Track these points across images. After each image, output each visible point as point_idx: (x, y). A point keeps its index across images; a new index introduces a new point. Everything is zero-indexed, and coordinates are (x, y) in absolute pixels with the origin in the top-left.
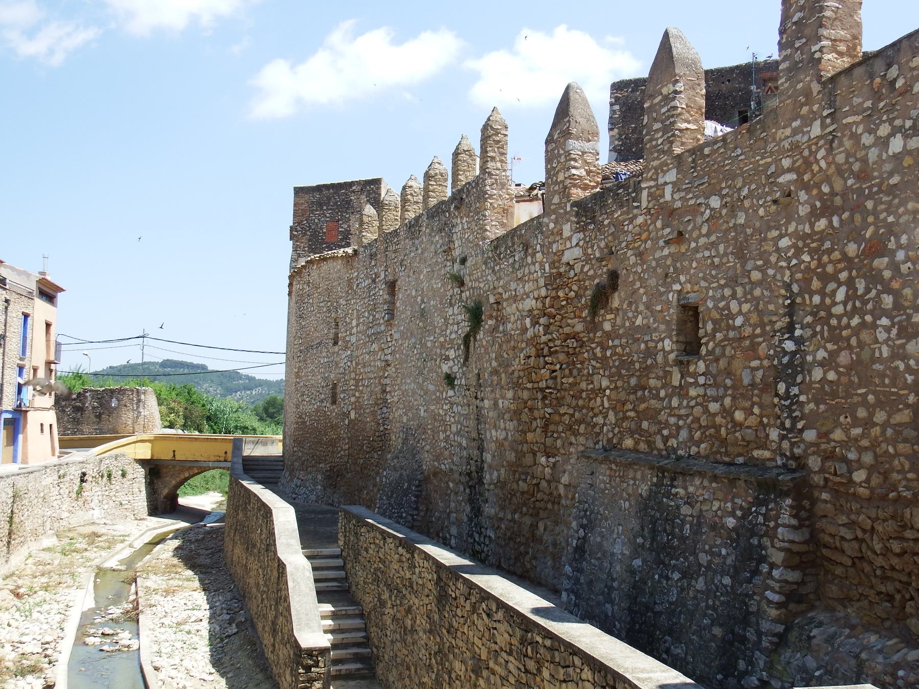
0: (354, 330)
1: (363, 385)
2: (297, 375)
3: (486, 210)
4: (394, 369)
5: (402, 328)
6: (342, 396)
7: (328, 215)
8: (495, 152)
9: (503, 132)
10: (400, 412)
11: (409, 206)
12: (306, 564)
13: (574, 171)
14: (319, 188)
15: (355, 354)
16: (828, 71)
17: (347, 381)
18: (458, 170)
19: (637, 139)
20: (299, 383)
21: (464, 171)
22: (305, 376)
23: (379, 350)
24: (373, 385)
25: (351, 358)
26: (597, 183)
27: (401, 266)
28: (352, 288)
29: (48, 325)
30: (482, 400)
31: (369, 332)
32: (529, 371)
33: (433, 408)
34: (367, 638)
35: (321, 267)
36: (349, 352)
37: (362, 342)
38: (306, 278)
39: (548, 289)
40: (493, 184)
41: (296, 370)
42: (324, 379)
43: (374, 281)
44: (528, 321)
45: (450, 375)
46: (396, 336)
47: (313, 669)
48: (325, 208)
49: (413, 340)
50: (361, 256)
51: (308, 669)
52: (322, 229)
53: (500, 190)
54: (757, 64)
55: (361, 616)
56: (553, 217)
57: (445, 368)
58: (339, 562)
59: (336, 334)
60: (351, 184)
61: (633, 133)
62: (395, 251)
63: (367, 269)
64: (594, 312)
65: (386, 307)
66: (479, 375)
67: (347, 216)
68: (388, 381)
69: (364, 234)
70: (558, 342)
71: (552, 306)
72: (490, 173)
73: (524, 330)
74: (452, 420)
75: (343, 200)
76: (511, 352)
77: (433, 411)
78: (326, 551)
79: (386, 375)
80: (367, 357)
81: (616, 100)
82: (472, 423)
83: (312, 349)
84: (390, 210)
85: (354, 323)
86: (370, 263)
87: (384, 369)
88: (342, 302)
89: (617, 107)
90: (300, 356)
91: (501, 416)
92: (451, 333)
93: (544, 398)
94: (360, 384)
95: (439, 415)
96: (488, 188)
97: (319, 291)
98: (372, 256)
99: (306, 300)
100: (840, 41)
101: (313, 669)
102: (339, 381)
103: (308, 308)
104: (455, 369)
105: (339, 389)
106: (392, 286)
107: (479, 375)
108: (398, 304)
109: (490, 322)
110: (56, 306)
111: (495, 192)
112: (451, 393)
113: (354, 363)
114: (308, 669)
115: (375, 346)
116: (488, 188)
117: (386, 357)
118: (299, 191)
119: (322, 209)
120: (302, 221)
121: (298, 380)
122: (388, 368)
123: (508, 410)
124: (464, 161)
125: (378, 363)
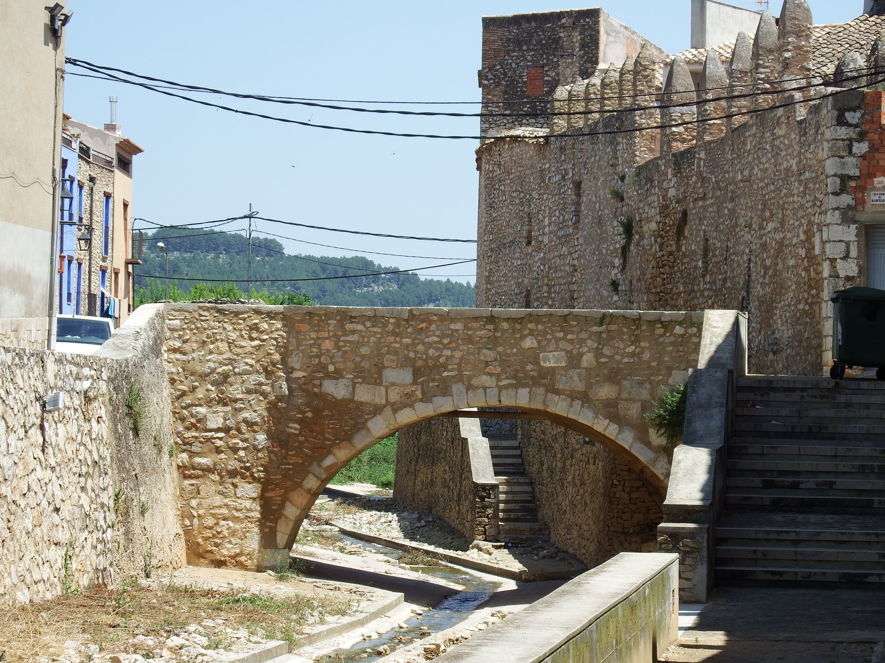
0: (547, 230)
1: (555, 292)
2: (488, 281)
3: (636, 137)
4: (579, 275)
5: (585, 233)
7: (529, 58)
8: (644, 86)
9: (650, 67)
11: (592, 105)
12: (485, 442)
14: (517, 20)
15: (547, 257)
16: (735, 125)
18: (623, 90)
20: (490, 290)
22: (497, 281)
23: (568, 254)
24: (563, 292)
26: (694, 137)
28: (544, 181)
29: (126, 206)
30: (633, 303)
31: (561, 233)
32: (654, 278)
34: (534, 497)
35: (512, 147)
37: (553, 243)
38: (497, 158)
39: (661, 216)
40: (642, 114)
41: (487, 274)
42: (519, 285)
44: (653, 239)
45: (615, 281)
47: (486, 499)
48: (525, 48)
50: (552, 146)
51: (482, 499)
52: (521, 77)
53: (649, 119)
55: (531, 484)
56: (664, 161)
58: (518, 452)
59: (530, 232)
60: (560, 15)
62: (581, 151)
63: (557, 162)
64: (679, 240)
65: (573, 209)
67: (555, 60)
68: (575, 287)
69: (556, 121)
70: (665, 258)
75: (549, 38)
78: (505, 443)
83: (505, 248)
85: (547, 221)
86: (561, 157)
88: (535, 195)
90: (491, 256)
93: (660, 300)
96: (637, 118)
97: (511, 177)
99: (497, 186)
100: (743, 107)
101: (486, 499)
102: (532, 287)
103: (499, 197)
105: (533, 297)
106: (578, 185)
108: (583, 208)
110: (131, 177)
111: (644, 121)
112: (616, 298)
113: (547, 266)
114: (482, 499)
116: (637, 118)
118: (489, 24)
119: (521, 50)
120: (495, 66)
121: (489, 286)
122: (576, 274)
125: (567, 268)
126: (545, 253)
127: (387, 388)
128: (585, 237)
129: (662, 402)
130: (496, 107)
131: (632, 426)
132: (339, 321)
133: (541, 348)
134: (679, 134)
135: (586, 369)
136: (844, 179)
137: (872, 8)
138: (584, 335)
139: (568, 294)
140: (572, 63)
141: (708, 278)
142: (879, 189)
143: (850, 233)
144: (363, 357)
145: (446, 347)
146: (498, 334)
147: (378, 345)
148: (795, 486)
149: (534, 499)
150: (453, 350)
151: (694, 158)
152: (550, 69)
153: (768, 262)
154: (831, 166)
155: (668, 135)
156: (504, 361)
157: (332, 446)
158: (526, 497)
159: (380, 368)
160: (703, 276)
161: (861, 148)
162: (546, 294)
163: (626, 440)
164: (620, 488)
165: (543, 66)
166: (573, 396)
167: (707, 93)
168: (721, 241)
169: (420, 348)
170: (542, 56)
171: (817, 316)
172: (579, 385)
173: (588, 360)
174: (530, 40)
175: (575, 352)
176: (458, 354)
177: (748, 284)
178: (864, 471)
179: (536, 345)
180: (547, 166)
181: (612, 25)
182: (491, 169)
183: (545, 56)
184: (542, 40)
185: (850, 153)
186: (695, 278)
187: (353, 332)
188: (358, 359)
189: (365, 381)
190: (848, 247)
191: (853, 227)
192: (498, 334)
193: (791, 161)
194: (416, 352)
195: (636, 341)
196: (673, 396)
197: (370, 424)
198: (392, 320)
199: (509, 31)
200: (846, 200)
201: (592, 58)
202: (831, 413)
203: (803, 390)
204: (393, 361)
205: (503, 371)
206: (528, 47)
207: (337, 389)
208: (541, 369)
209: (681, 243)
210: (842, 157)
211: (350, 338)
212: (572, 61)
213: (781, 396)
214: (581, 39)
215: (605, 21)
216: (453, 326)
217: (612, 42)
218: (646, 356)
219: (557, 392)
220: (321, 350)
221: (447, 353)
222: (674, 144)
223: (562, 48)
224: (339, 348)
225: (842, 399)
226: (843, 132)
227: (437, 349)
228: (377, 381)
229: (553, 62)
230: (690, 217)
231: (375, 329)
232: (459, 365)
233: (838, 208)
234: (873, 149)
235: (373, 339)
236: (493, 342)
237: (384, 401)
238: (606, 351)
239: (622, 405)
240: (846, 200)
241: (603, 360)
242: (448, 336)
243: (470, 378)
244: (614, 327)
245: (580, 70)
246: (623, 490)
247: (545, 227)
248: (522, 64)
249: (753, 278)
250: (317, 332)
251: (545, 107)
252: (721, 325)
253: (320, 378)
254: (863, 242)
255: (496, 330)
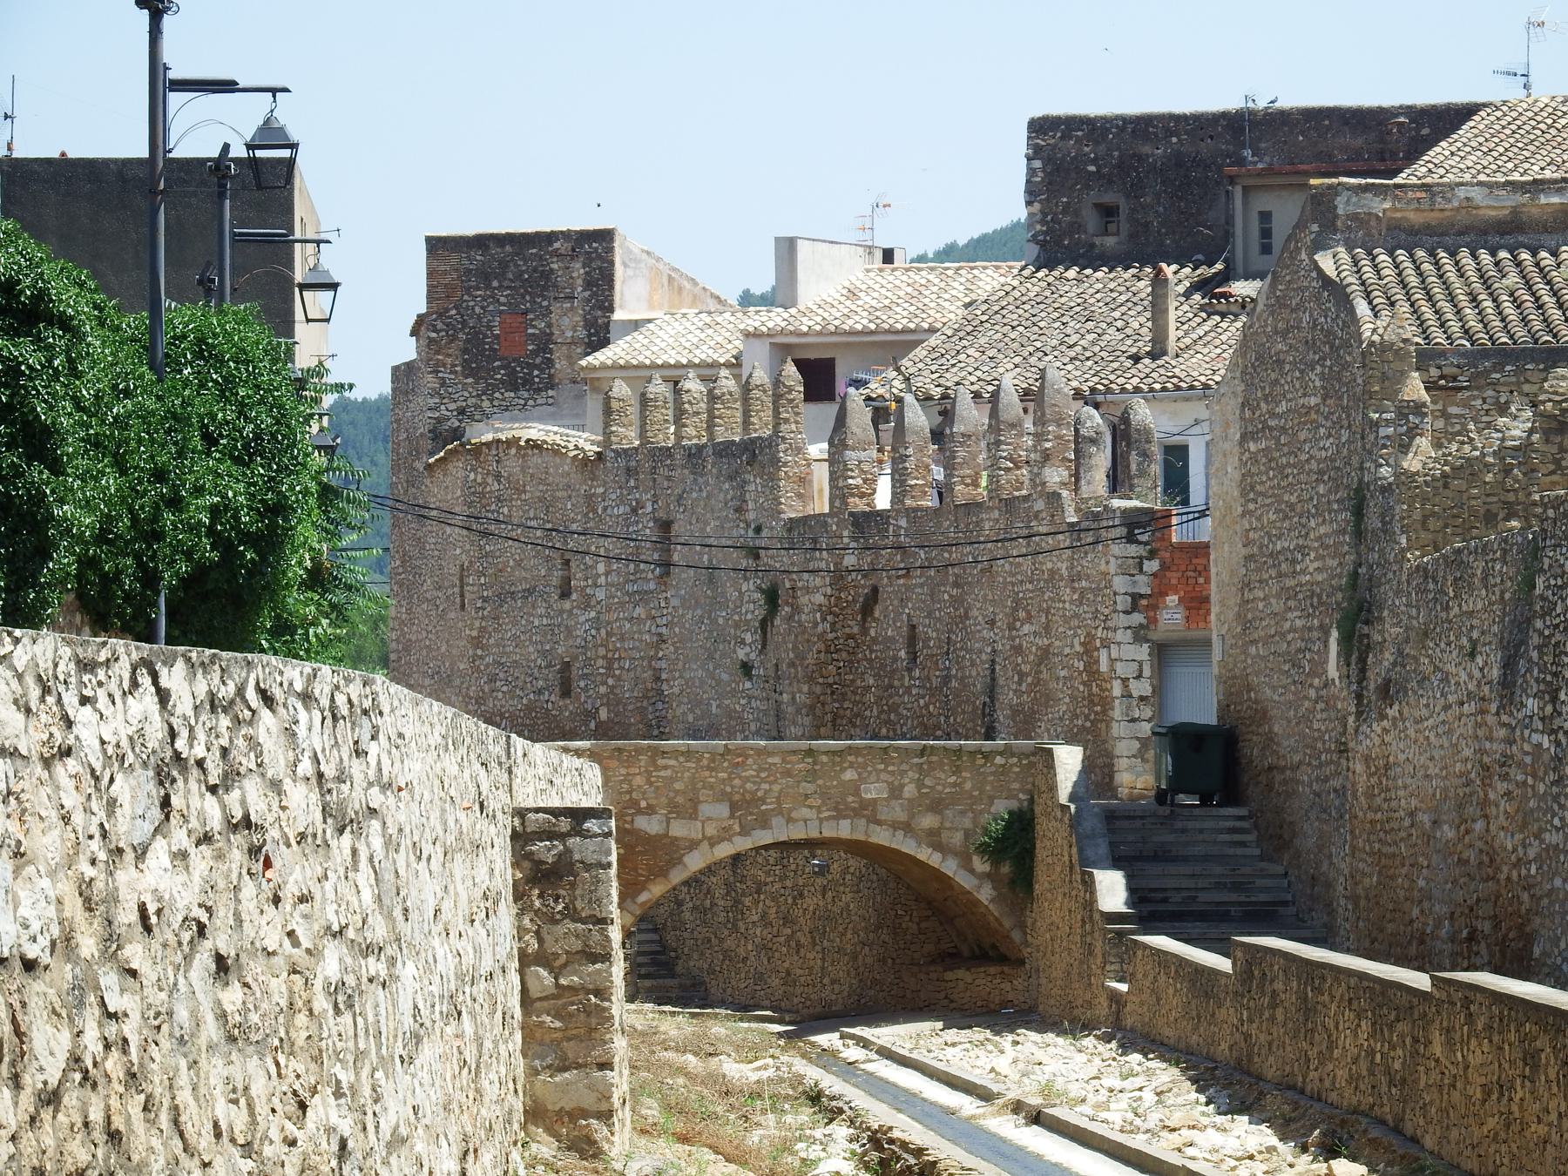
0: (602, 580)
1: (622, 668)
5: (683, 592)
6: (582, 684)
7: (503, 299)
10: (684, 708)
13: (850, 481)
17: (590, 659)
19: (1071, 224)
21: (757, 411)
25: (597, 623)
27: (679, 505)
28: (595, 511)
30: (781, 694)
31: (630, 588)
32: (820, 665)
33: (727, 702)
36: (593, 614)
42: (543, 654)
43: (634, 511)
44: (818, 615)
46: (675, 602)
48: (495, 284)
49: (699, 612)
50: (608, 464)
52: (490, 328)
54: (1252, 113)
57: (741, 654)
60: (551, 237)
61: (1064, 212)
62: (669, 478)
64: (864, 620)
66: (777, 665)
67: (545, 303)
69: (614, 429)
70: (841, 641)
71: (836, 606)
72: (784, 438)
73: (816, 624)
74: (751, 716)
75: (535, 270)
76: (805, 645)
77: (727, 706)
79: (660, 655)
80: (628, 626)
81: (1035, 153)
82: (772, 720)
84: (656, 407)
87: (657, 648)
89: (1037, 164)
91: (798, 711)
92: (747, 612)
93: (833, 693)
94: (616, 666)
95: (735, 711)
96: (781, 455)
98: (629, 472)
102: (575, 658)
104: (753, 656)
105: (575, 672)
107: (777, 665)
109: (786, 609)
112: (748, 685)
113: (603, 632)
115: (639, 611)
116: (781, 455)
117: (660, 630)
118: (436, 246)
119: (488, 287)
120: (447, 310)
121: (479, 652)
122: (664, 646)
123: (805, 705)
124: (757, 399)
125: (647, 637)
126: (599, 613)
127: (703, 823)
128: (683, 598)
129: (986, 832)
130: (451, 373)
131: (956, 854)
132: (651, 757)
133: (862, 780)
134: (857, 487)
135: (909, 799)
136: (1135, 597)
137: (1038, 257)
138: (904, 767)
139: (650, 672)
140: (572, 309)
141: (917, 673)
142: (1171, 608)
143: (1143, 652)
144: (677, 792)
145: (763, 780)
146: (817, 767)
147: (693, 778)
148: (1165, 900)
149: (665, 949)
150: (771, 783)
151: (888, 523)
152: (537, 318)
153: (1026, 668)
154: (1120, 584)
155: (842, 488)
156: (824, 795)
157: (646, 882)
158: (655, 948)
159: (695, 803)
160: (909, 670)
161: (1152, 566)
162: (602, 671)
163: (950, 867)
164: (907, 918)
165: (525, 313)
166: (895, 826)
167: (907, 448)
168: (937, 630)
169: (737, 782)
170: (524, 298)
171: (1103, 734)
172: (902, 816)
173: (910, 791)
174: (504, 273)
175: (896, 783)
176: (776, 788)
177: (992, 690)
178: (1219, 886)
179: (856, 777)
180: (601, 490)
181: (631, 252)
182: (479, 480)
183: (528, 298)
184: (524, 272)
185: (1141, 570)
186: (894, 671)
187: (666, 767)
188: (672, 794)
189: (679, 816)
190: (1141, 666)
191: (1146, 646)
192: (817, 767)
193: (1059, 564)
194: (732, 787)
195: (957, 771)
196: (997, 824)
197: (686, 859)
198: (706, 755)
199: (468, 258)
200: (1138, 618)
201: (603, 302)
202: (1170, 838)
203: (1142, 818)
204: (709, 796)
205: (824, 803)
206: (500, 282)
207: (650, 825)
208: (862, 800)
209: (867, 625)
210: (1133, 575)
211: (662, 773)
212: (572, 307)
213: (1125, 824)
214: (586, 273)
215: (621, 246)
216: (770, 760)
217: (631, 277)
218: (968, 786)
219: (879, 823)
220: (631, 786)
221: (765, 786)
222: (851, 500)
223: (555, 286)
224: (651, 784)
225: (1179, 825)
226: (1133, 550)
227: (754, 783)
228: (693, 816)
229: (541, 307)
230: (882, 596)
231: (689, 764)
232: (778, 798)
233: (1129, 627)
234: (1164, 567)
235: (687, 774)
236: (812, 775)
237: (700, 836)
238: (928, 782)
239: (945, 835)
240: (1138, 618)
241: (924, 791)
242: (766, 769)
243: (790, 810)
244: (934, 758)
245: (585, 320)
246: (911, 920)
247: (599, 576)
248: (491, 308)
249: (1001, 681)
250: (627, 767)
251: (530, 374)
252: (1070, 761)
253: (632, 815)
254: (1156, 662)
255: (815, 763)
